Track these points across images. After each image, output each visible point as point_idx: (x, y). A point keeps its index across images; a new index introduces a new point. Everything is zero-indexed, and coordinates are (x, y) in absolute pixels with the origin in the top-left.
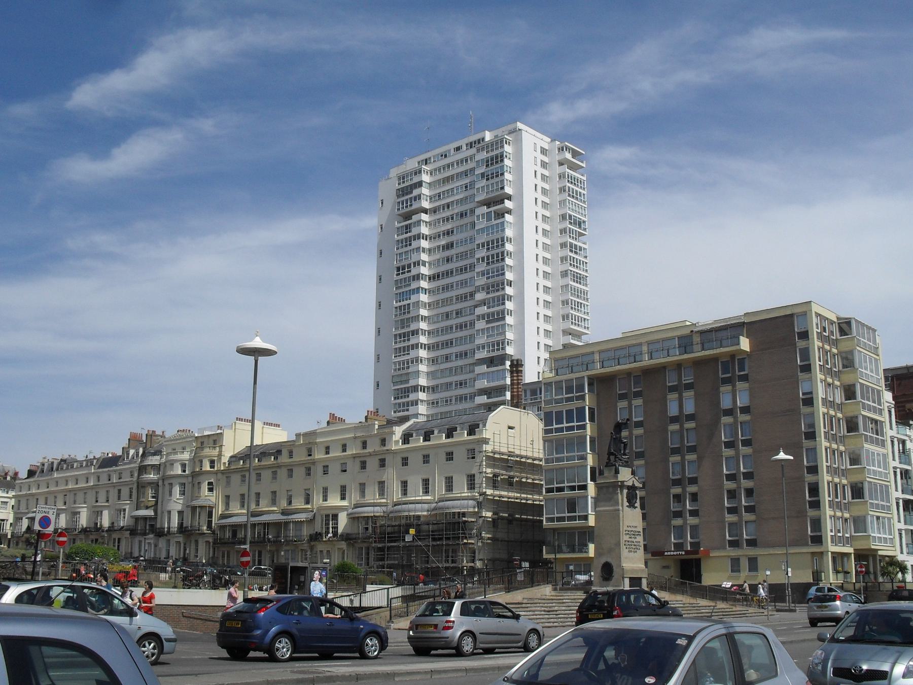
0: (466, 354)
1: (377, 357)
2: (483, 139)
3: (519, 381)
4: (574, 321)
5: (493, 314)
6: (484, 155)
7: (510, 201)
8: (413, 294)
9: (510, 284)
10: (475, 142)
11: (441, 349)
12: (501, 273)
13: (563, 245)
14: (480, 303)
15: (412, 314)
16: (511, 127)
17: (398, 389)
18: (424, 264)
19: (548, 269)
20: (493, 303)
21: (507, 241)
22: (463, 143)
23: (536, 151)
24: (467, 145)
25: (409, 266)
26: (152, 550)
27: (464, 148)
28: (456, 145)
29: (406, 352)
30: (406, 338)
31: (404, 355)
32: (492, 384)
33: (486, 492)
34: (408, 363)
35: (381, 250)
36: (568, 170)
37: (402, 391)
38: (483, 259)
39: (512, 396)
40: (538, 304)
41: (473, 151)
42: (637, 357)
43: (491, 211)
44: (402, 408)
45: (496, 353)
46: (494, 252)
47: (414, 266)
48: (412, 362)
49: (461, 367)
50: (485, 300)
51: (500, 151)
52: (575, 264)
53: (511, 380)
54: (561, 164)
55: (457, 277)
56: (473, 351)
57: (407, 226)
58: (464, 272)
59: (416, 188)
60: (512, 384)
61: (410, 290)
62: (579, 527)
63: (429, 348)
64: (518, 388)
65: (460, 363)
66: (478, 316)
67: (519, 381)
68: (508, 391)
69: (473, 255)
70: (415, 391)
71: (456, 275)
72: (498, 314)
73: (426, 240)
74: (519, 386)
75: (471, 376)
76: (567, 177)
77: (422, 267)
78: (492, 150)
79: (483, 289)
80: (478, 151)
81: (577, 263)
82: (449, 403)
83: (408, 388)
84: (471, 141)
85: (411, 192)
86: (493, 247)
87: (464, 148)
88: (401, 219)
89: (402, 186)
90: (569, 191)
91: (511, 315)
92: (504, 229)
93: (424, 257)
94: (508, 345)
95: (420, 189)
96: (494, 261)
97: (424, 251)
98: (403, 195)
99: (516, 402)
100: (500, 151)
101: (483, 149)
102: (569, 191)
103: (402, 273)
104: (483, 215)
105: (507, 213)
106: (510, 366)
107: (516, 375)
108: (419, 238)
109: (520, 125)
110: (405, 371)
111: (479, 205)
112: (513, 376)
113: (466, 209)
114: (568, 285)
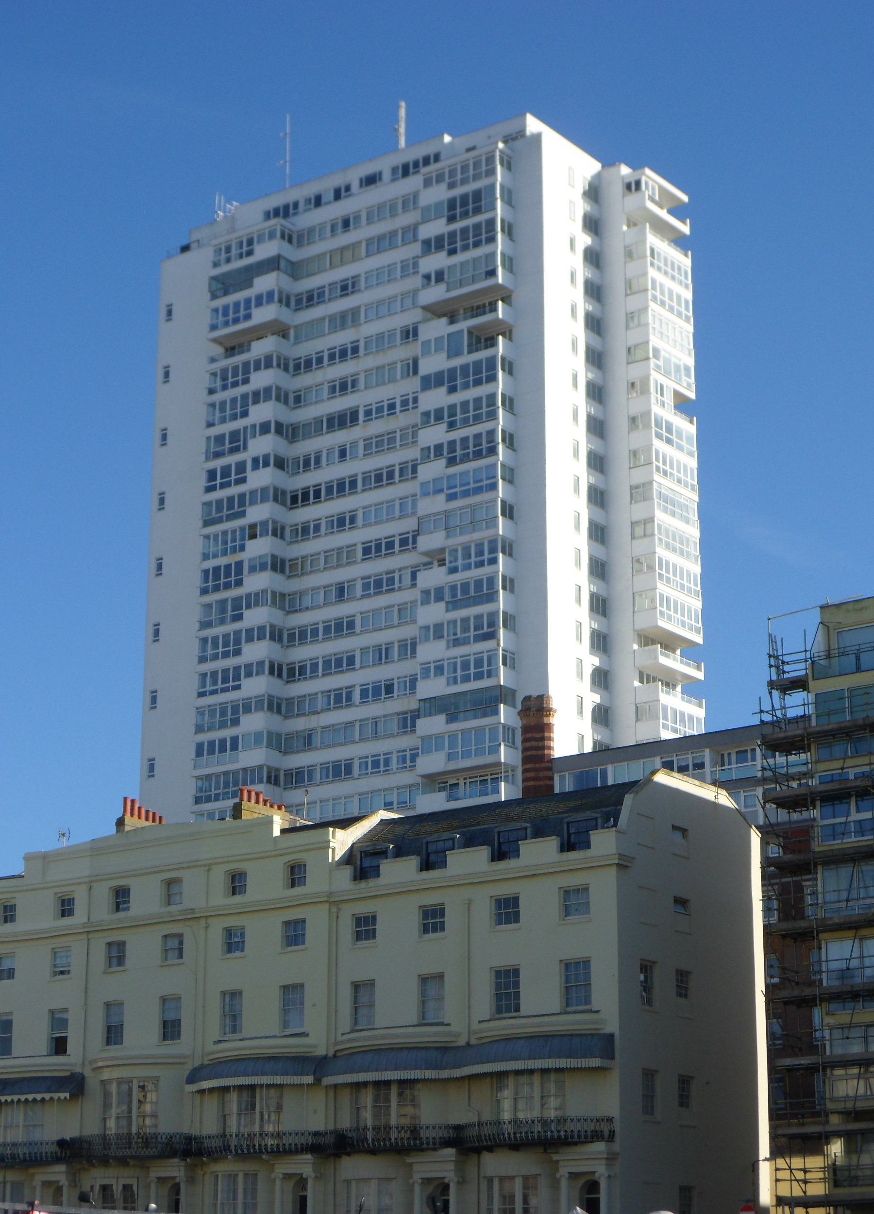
0: (389, 689)
5: (465, 586)
6: (439, 194)
10: (416, 164)
11: (323, 675)
14: (426, 559)
17: (209, 777)
20: (464, 558)
23: (573, 187)
25: (241, 467)
26: (698, 755)
28: (368, 169)
29: (231, 684)
30: (233, 578)
31: (224, 690)
34: (237, 642)
37: (217, 783)
38: (439, 448)
41: (414, 182)
42: (863, 656)
43: (462, 331)
44: (220, 685)
46: (469, 431)
49: (375, 722)
50: (442, 550)
55: (366, 494)
57: (235, 436)
58: (385, 482)
62: (796, 1134)
65: (375, 709)
66: (426, 593)
71: (363, 491)
72: (479, 583)
75: (406, 742)
80: (427, 183)
82: (382, 768)
83: (235, 773)
88: (219, 350)
89: (225, 268)
96: (469, 453)
98: (226, 293)
101: (440, 178)
102: (654, 288)
103: (223, 486)
111: (429, 315)
113: (330, 537)
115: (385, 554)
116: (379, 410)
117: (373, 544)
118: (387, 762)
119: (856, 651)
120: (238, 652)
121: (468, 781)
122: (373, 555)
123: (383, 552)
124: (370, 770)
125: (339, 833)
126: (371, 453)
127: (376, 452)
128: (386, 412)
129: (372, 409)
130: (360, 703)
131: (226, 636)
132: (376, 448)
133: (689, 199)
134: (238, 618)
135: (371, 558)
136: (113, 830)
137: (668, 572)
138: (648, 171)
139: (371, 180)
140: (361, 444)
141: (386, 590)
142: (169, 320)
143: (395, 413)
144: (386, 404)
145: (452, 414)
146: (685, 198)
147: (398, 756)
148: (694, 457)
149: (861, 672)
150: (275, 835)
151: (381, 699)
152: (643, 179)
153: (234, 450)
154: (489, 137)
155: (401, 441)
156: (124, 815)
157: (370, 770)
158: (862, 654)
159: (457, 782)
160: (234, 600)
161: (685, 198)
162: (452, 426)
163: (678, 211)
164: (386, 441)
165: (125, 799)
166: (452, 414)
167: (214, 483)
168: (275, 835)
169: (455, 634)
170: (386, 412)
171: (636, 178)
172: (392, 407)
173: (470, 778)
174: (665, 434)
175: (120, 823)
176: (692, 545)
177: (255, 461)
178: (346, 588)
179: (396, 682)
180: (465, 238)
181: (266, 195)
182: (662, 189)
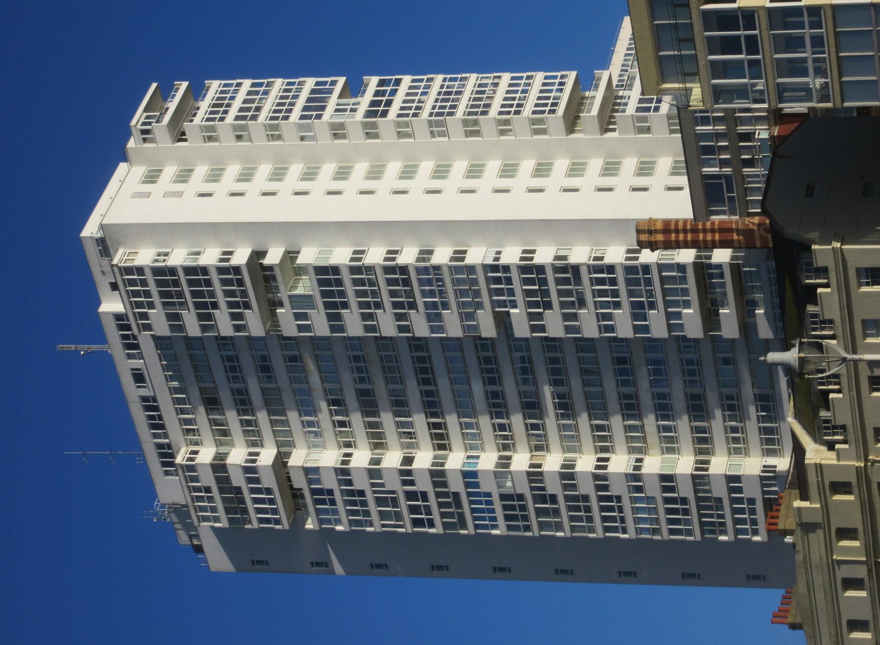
1: (376, 570)
2: (118, 317)
3: (689, 227)
4: (513, 110)
7: (298, 252)
8: (446, 487)
9: (459, 255)
12: (644, 273)
13: (371, 132)
15: (524, 488)
16: (92, 253)
18: (408, 460)
19: (527, 165)
21: (360, 259)
22: (125, 366)
24: (130, 357)
25: (410, 496)
27: (138, 363)
32: (693, 296)
33: (281, 304)
35: (748, 577)
36: (197, 120)
39: (724, 244)
40: (576, 190)
41: (145, 340)
45: (691, 284)
47: (412, 483)
48: (606, 488)
51: (149, 277)
52: (414, 105)
53: (686, 245)
54: (181, 137)
56: (613, 344)
57: (380, 502)
59: (227, 479)
60: (694, 244)
61: (469, 494)
63: (707, 452)
64: (705, 231)
67: (689, 227)
68: (710, 257)
69: (357, 342)
70: (542, 481)
73: (607, 460)
74: (700, 227)
76: (244, 122)
77: (416, 465)
78: (148, 294)
79: (471, 316)
81: (546, 105)
84: (142, 346)
85: (238, 490)
86: (374, 294)
87: (138, 363)
90: (244, 118)
91: (533, 252)
92: (678, 264)
93: (392, 459)
94: (601, 259)
95: (230, 469)
97: (377, 461)
99: (738, 235)
100: (149, 277)
103: (429, 513)
104: (298, 316)
105: (293, 259)
106: (653, 250)
107: (673, 235)
108: (442, 474)
109: (90, 230)
110: (759, 506)
112: (713, 241)
114: (430, 122)
115: (496, 364)
116: (359, 370)
117: (486, 376)
118: (690, 362)
119: (683, 76)
120: (586, 498)
121: (708, 290)
122: (484, 366)
123: (493, 366)
124: (697, 378)
125: (808, 455)
126: (400, 377)
127: (399, 373)
128: (362, 364)
129: (358, 377)
130: (634, 386)
131: (570, 509)
132: (396, 373)
133: (155, 82)
134: (553, 499)
135: (481, 364)
136: (799, 633)
137: (511, 106)
138: (133, 123)
139: (139, 377)
140: (391, 386)
141: (529, 364)
142: (267, 563)
143: (363, 356)
144: (354, 365)
145: (367, 305)
146: (154, 86)
147: (685, 353)
148: (401, 79)
149: (699, 72)
150: (859, 545)
151: (631, 368)
152: (139, 126)
153: (395, 502)
154: (103, 273)
155: (390, 351)
156: (786, 624)
157: (697, 378)
158: (685, 72)
159: (709, 300)
160: (535, 502)
161: (154, 86)
162: (378, 305)
163: (165, 93)
164: (390, 364)
165: (772, 623)
166: (367, 305)
167: (156, 417)
168: (859, 545)
169: (573, 303)
170: (362, 364)
171: (139, 133)
172: (357, 359)
173: (706, 289)
174: (381, 108)
175: (794, 626)
176: (484, 81)
177: (405, 483)
178: (526, 400)
179: (615, 355)
180: (200, 294)
181: (440, 568)
182: (146, 110)
